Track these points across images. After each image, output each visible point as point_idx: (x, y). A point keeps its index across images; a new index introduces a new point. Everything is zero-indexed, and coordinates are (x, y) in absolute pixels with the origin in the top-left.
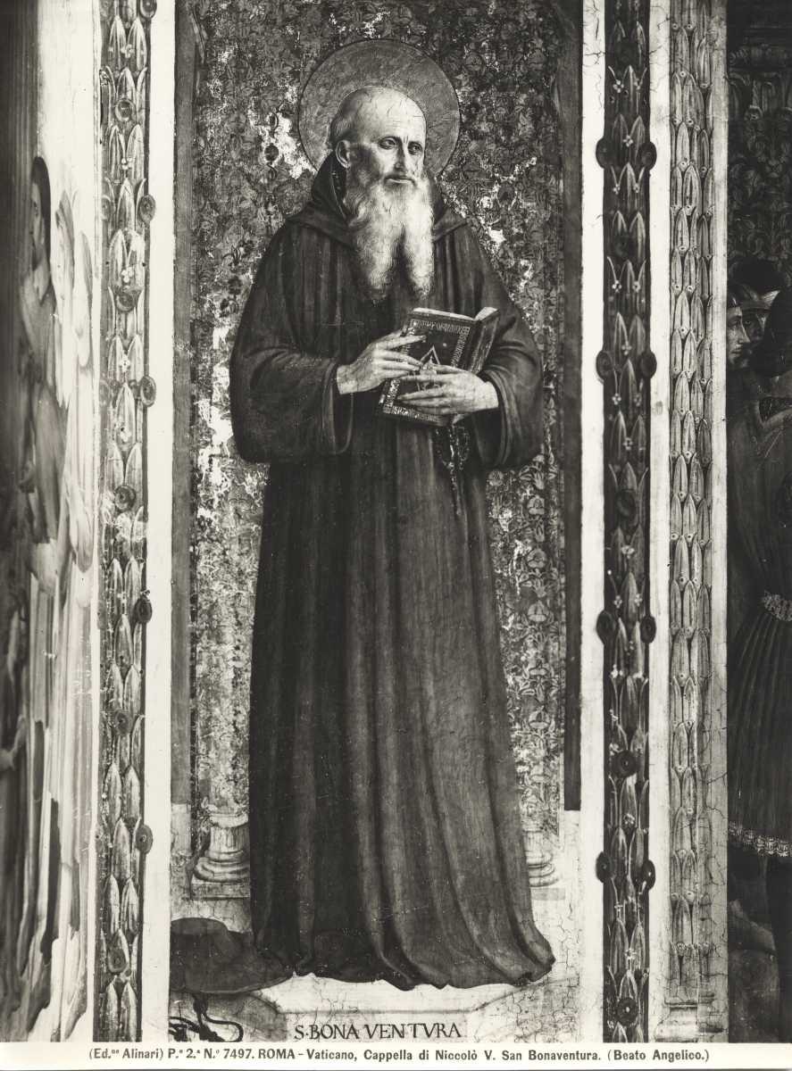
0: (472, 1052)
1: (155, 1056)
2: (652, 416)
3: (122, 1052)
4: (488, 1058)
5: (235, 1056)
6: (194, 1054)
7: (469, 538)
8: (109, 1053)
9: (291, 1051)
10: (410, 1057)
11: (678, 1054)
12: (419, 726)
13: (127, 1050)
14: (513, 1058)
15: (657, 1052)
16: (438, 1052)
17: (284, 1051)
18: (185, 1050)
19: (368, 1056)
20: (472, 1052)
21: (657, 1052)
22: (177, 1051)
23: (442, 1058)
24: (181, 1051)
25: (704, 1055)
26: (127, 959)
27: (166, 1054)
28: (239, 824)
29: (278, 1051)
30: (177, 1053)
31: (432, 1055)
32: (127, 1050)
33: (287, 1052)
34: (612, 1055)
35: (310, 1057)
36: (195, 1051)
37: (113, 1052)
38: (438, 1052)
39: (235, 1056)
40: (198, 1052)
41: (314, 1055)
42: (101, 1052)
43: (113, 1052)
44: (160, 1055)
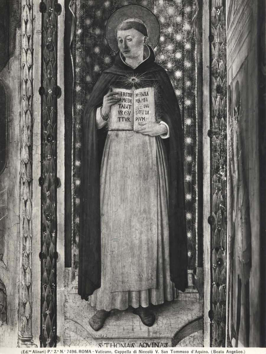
0: (222, 351)
1: (43, 352)
2: (209, 95)
3: (32, 351)
4: (157, 352)
5: (71, 352)
6: (57, 352)
7: (195, 98)
8: (28, 352)
9: (90, 350)
10: (130, 352)
11: (235, 351)
12: (46, 185)
13: (34, 351)
14: (165, 352)
15: (228, 351)
16: (140, 351)
17: (88, 350)
18: (53, 350)
19: (116, 352)
20: (151, 351)
21: (228, 351)
22: (51, 351)
23: (141, 353)
24: (52, 351)
25: (243, 352)
26: (214, 313)
27: (47, 352)
28: (253, 261)
29: (86, 350)
30: (51, 351)
31: (138, 352)
32: (34, 351)
33: (89, 351)
34: (213, 352)
35: (97, 352)
36: (57, 351)
37: (29, 351)
38: (140, 351)
39: (71, 352)
40: (58, 351)
41: (98, 352)
42: (25, 351)
43: (29, 351)
44: (45, 352)
